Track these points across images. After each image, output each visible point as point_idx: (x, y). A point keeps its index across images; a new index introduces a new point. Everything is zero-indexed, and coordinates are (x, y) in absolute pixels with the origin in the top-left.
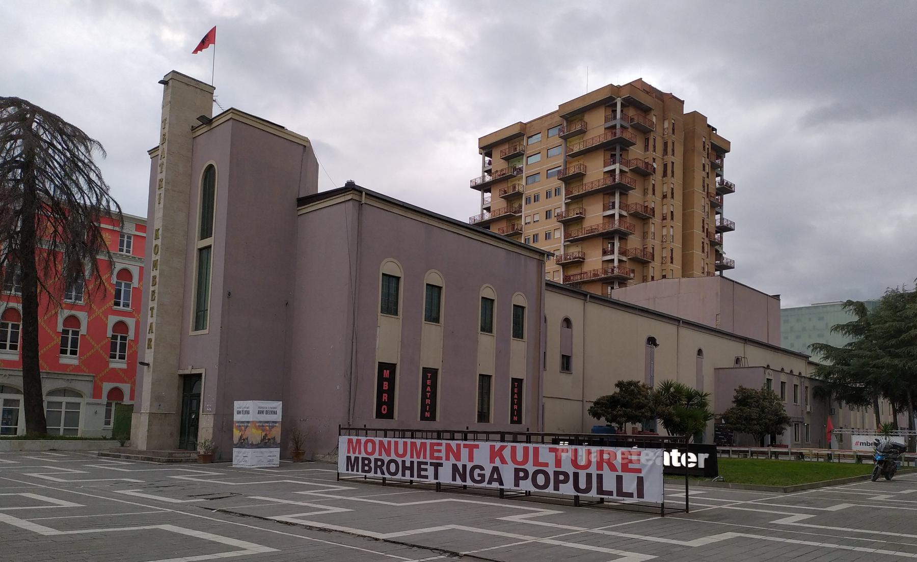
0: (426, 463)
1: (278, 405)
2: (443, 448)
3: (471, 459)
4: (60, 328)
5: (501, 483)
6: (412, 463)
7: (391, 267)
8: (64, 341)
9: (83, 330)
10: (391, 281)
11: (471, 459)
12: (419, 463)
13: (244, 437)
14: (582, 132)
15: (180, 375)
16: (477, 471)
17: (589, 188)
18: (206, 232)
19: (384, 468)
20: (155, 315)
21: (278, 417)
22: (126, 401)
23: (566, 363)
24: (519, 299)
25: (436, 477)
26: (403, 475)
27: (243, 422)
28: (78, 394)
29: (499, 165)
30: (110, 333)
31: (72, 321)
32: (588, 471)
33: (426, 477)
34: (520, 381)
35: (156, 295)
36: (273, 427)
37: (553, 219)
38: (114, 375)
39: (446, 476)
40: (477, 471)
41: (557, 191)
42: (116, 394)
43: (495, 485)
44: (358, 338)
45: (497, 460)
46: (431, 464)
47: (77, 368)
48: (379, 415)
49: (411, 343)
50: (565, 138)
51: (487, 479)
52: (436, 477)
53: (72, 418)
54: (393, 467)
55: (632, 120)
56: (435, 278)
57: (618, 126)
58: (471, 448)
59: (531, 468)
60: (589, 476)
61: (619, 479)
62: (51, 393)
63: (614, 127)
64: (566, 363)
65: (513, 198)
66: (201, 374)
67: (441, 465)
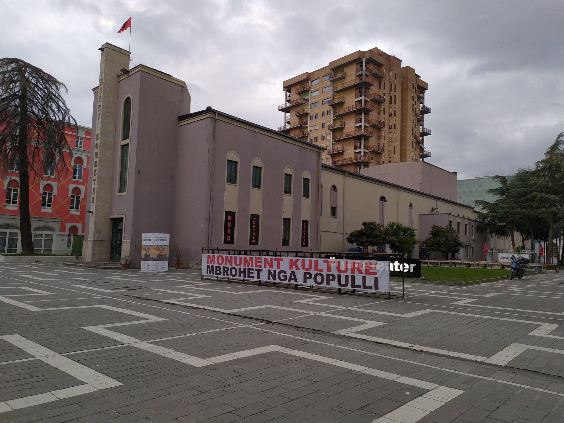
0: (253, 269)
1: (167, 236)
2: (263, 261)
3: (279, 267)
4: (41, 191)
5: (296, 281)
6: (245, 269)
7: (232, 156)
8: (44, 199)
9: (55, 192)
10: (232, 164)
11: (279, 267)
12: (249, 270)
13: (148, 254)
14: (343, 78)
15: (111, 219)
16: (282, 274)
17: (346, 111)
18: (126, 136)
19: (229, 272)
20: (96, 184)
21: (167, 243)
22: (80, 233)
23: (334, 212)
24: (307, 175)
25: (259, 277)
26: (240, 276)
27: (147, 246)
28: (52, 230)
29: (295, 97)
30: (70, 194)
31: (49, 187)
32: (346, 274)
33: (253, 277)
34: (307, 222)
35: (97, 172)
36: (164, 248)
37: (326, 129)
38: (73, 219)
39: (264, 277)
40: (282, 274)
41: (328, 112)
42: (74, 229)
43: (293, 282)
44: (214, 197)
45: (294, 267)
46: (256, 270)
47: (51, 215)
48: (226, 242)
49: (244, 200)
50: (333, 82)
51: (288, 278)
52: (259, 277)
53: (49, 244)
54: (233, 272)
55: (372, 71)
56: (258, 162)
57: (364, 75)
58: (279, 261)
59: (313, 272)
60: (347, 277)
61: (364, 279)
62: (36, 229)
63: (361, 75)
64: (334, 212)
65: (303, 116)
66: (122, 218)
67: (261, 270)
